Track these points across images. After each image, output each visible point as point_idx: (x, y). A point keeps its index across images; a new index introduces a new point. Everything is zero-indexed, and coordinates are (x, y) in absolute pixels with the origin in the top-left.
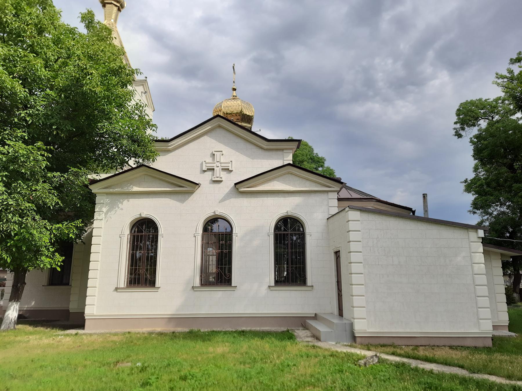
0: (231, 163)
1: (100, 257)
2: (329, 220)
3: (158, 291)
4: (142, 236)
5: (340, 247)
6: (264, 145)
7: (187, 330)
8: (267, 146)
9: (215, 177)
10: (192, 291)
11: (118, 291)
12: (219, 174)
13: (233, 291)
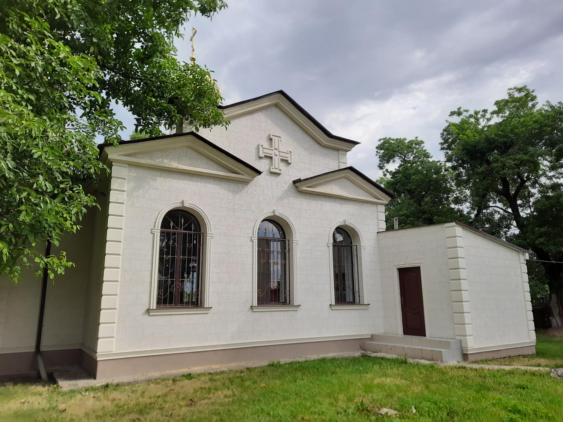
0: (290, 153)
1: (121, 261)
2: (379, 234)
3: (208, 313)
4: (190, 235)
5: (422, 263)
6: (324, 140)
7: (265, 363)
8: (327, 142)
9: (273, 167)
10: (251, 312)
11: (150, 314)
12: (278, 165)
13: (295, 312)
